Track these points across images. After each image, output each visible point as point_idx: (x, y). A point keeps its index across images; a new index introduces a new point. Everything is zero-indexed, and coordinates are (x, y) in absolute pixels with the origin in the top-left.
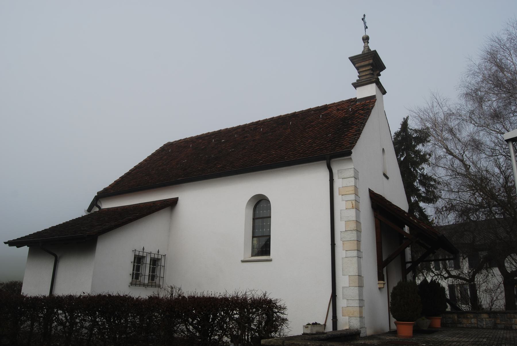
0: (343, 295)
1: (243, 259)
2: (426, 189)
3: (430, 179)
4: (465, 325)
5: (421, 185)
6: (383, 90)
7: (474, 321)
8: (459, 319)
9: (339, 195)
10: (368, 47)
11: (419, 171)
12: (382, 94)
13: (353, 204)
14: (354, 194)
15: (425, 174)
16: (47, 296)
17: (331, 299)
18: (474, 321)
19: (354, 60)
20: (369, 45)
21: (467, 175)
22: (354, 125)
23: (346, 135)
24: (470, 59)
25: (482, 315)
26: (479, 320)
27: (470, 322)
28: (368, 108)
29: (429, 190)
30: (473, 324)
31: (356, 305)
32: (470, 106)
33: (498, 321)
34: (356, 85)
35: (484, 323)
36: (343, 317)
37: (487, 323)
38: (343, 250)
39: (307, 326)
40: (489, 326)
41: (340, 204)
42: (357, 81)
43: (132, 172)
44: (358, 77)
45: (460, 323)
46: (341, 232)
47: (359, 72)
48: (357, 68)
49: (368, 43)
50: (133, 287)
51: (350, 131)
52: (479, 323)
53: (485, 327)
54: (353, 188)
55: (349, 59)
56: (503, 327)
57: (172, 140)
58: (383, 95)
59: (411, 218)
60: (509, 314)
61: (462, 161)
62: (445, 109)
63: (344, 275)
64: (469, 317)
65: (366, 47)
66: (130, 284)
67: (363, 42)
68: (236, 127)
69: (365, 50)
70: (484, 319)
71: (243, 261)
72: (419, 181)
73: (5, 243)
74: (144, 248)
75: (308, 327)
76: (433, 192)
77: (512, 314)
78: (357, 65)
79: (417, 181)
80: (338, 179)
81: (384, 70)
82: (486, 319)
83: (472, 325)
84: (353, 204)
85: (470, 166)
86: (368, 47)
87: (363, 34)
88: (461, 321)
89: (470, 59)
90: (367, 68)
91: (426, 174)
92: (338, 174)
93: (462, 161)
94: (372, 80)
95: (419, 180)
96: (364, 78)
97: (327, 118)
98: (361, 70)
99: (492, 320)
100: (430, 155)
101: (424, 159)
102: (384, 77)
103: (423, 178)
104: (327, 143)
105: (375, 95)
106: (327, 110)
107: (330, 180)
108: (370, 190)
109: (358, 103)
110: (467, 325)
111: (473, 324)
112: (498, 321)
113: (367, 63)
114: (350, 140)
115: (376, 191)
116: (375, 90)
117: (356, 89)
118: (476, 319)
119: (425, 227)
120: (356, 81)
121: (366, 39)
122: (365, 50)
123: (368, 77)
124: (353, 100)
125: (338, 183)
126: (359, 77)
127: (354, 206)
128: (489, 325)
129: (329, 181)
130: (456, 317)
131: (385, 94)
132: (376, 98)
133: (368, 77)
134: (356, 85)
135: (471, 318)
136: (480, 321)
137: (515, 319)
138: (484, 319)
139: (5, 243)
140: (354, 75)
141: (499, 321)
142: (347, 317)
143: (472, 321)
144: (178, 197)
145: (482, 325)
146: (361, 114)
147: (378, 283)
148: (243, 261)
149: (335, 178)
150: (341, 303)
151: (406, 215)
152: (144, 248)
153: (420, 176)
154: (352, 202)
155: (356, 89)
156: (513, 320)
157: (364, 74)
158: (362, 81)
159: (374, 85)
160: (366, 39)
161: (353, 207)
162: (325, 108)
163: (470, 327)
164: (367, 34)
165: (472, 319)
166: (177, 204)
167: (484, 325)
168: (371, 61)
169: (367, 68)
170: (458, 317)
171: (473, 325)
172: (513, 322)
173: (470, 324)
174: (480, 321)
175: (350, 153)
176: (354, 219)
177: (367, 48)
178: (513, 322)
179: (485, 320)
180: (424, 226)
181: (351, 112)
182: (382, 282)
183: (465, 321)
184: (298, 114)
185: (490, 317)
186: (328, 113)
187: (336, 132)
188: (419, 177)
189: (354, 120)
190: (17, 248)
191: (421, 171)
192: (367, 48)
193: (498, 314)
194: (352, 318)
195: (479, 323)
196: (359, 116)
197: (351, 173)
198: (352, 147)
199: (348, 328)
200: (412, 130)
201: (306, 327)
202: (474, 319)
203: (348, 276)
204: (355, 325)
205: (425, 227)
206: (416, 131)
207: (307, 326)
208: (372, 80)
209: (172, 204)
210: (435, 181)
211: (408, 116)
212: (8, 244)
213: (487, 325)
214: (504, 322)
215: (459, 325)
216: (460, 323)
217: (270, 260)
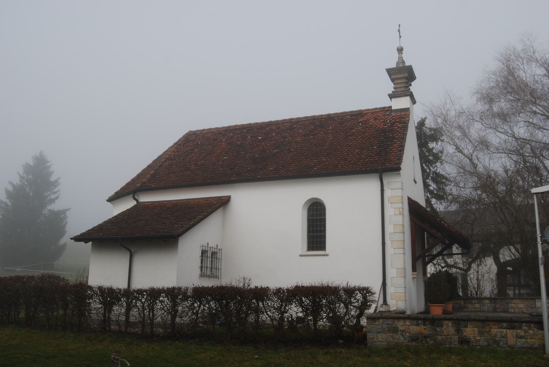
0: (391, 283)
1: (300, 253)
2: (437, 186)
3: (443, 177)
4: (470, 309)
5: (433, 182)
6: (414, 101)
7: (477, 306)
8: (465, 304)
9: (389, 203)
10: (402, 59)
11: (432, 169)
12: (412, 104)
13: (400, 211)
14: (402, 203)
15: (438, 172)
16: (125, 288)
17: (381, 287)
18: (478, 306)
19: (390, 72)
20: (403, 55)
21: (474, 173)
22: (396, 139)
23: (391, 150)
24: (486, 66)
25: (485, 300)
26: (482, 305)
27: (474, 307)
28: (405, 122)
29: (440, 187)
30: (476, 308)
31: (402, 292)
32: (480, 107)
33: (498, 306)
34: (392, 96)
35: (486, 308)
36: (392, 301)
37: (488, 308)
38: (392, 248)
39: (382, 306)
40: (490, 310)
41: (389, 211)
42: (393, 92)
43: (163, 163)
44: (394, 88)
45: (466, 308)
46: (390, 233)
47: (394, 84)
48: (393, 80)
49: (402, 53)
50: (203, 278)
51: (394, 146)
52: (482, 308)
53: (486, 311)
54: (400, 198)
55: (386, 70)
56: (501, 311)
57: (194, 129)
58: (414, 105)
59: (443, 222)
60: (506, 300)
61: (471, 160)
62: (457, 107)
63: (393, 268)
64: (473, 302)
65: (400, 58)
66: (200, 276)
67: (398, 53)
68: (266, 123)
69: (400, 61)
70: (486, 304)
71: (301, 256)
72: (431, 178)
73: (71, 239)
74: (217, 245)
75: (383, 307)
76: (444, 189)
77: (509, 300)
78: (393, 77)
79: (430, 178)
80: (388, 189)
81: (415, 81)
82: (488, 304)
83: (476, 309)
84: (400, 211)
85: (477, 165)
86: (402, 59)
87: (398, 45)
88: (467, 306)
89: (486, 66)
90: (402, 81)
91: (439, 172)
92: (387, 185)
93: (471, 160)
94: (407, 93)
95: (431, 177)
96: (399, 90)
97: (367, 127)
98: (396, 82)
99: (492, 305)
100: (442, 152)
101: (437, 157)
102: (414, 87)
103: (435, 175)
104: (376, 156)
105: (409, 108)
106: (363, 116)
107: (381, 190)
108: (408, 197)
109: (393, 114)
110: (472, 309)
111: (476, 308)
112: (498, 306)
113: (402, 76)
114: (396, 156)
115: (409, 197)
116: (409, 103)
117: (391, 100)
118: (479, 304)
119: (454, 230)
120: (392, 93)
121: (400, 50)
122: (400, 61)
123: (403, 89)
124: (388, 109)
125: (387, 193)
126: (394, 88)
127: (401, 212)
128: (490, 309)
129: (380, 191)
130: (462, 303)
131: (415, 104)
132: (409, 110)
133: (403, 89)
134: (391, 96)
135: (475, 303)
136: (482, 306)
137: (511, 304)
138: (486, 304)
139: (71, 239)
140: (390, 87)
141: (498, 305)
142: (395, 301)
143: (476, 306)
144: (230, 196)
145: (484, 309)
146: (400, 128)
147: (412, 274)
148: (301, 256)
149: (385, 188)
150: (390, 290)
151: (438, 219)
152: (217, 245)
153: (433, 174)
154: (399, 209)
155: (391, 100)
156: (510, 304)
157: (399, 86)
158: (398, 93)
159: (408, 98)
160: (400, 50)
161: (400, 213)
162: (361, 114)
163: (474, 310)
164: (402, 45)
165: (476, 304)
166: (230, 202)
167: (485, 309)
168: (406, 75)
169: (402, 81)
170: (464, 303)
171: (477, 309)
172: (510, 306)
173: (474, 308)
174: (482, 306)
175: (399, 169)
176: (401, 223)
177: (401, 61)
178: (510, 306)
179: (487, 305)
180: (453, 229)
181: (388, 124)
182: (415, 273)
183: (470, 306)
184: (334, 117)
185: (491, 303)
186: (365, 121)
187: (360, 131)
188: (431, 175)
189: (394, 133)
190: (85, 243)
191: (434, 169)
192: (401, 61)
193: (498, 300)
194: (399, 301)
195: (482, 308)
196: (399, 130)
197: (399, 185)
198: (400, 163)
199: (395, 309)
200: (427, 128)
201: (381, 307)
202: (478, 304)
203: (396, 269)
204: (401, 307)
205: (454, 230)
206: (431, 129)
207: (382, 306)
208: (407, 93)
209: (224, 202)
210: (446, 179)
211: (426, 117)
212: (73, 240)
213: (489, 309)
214: (502, 307)
215: (465, 310)
216: (466, 308)
217: (327, 255)
